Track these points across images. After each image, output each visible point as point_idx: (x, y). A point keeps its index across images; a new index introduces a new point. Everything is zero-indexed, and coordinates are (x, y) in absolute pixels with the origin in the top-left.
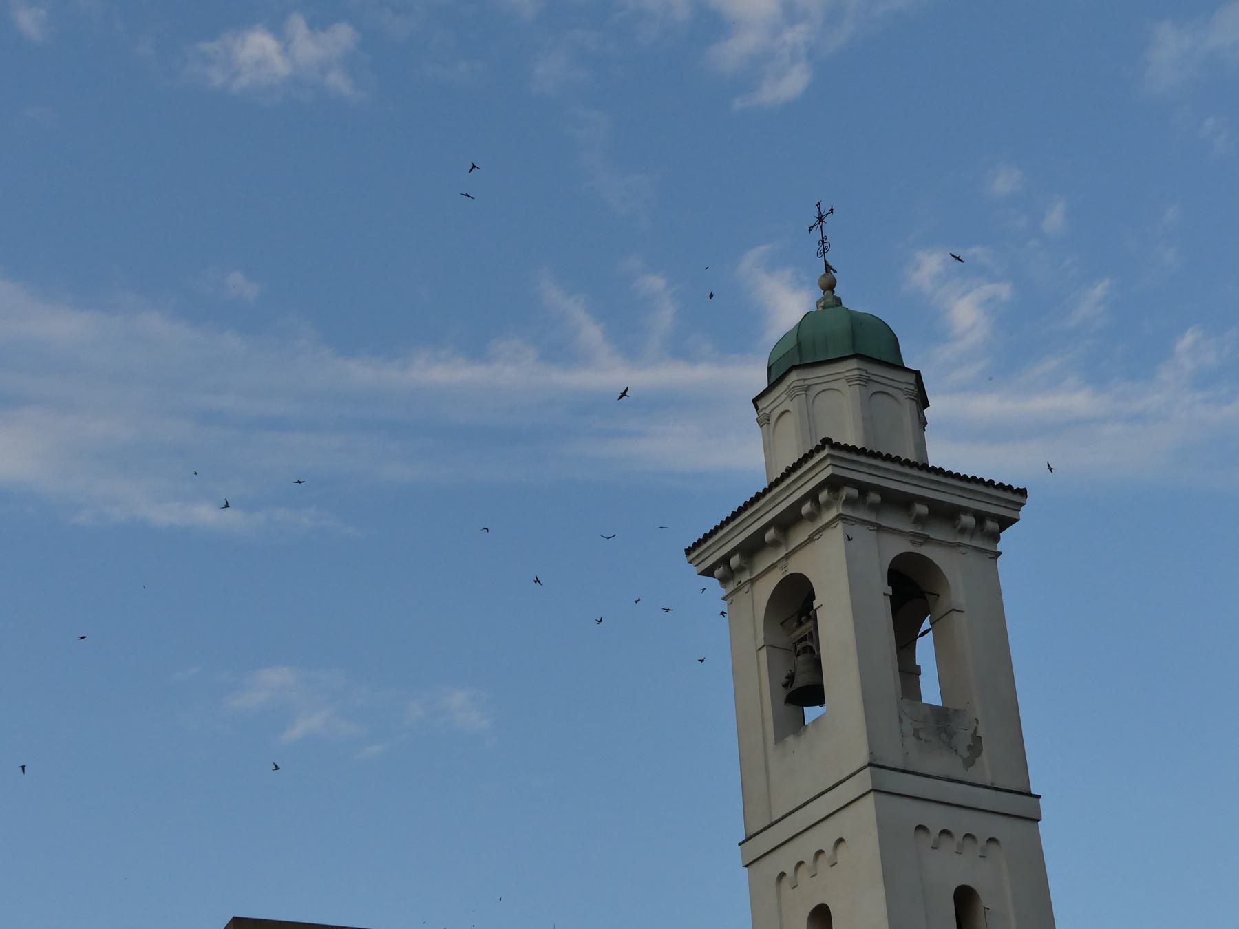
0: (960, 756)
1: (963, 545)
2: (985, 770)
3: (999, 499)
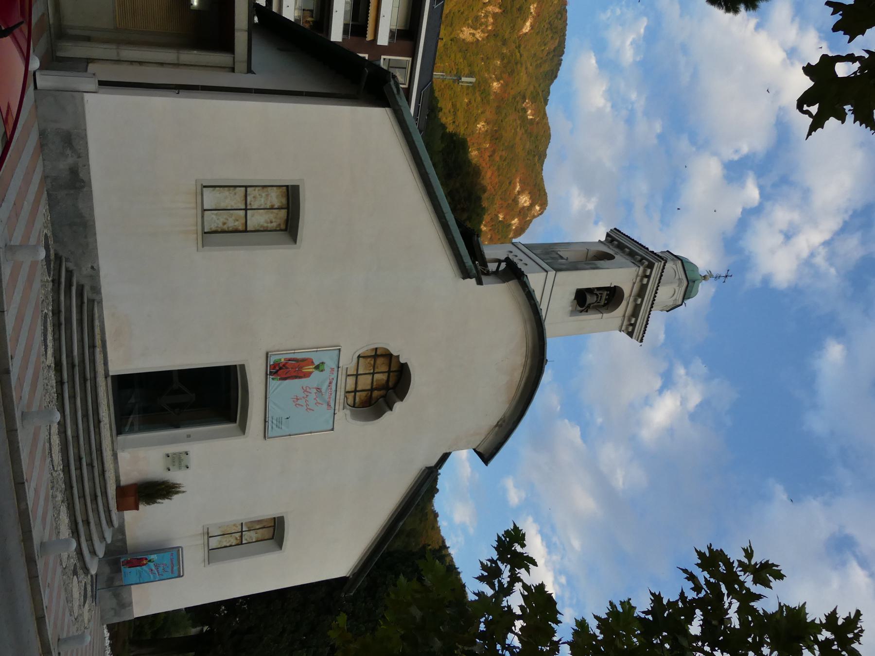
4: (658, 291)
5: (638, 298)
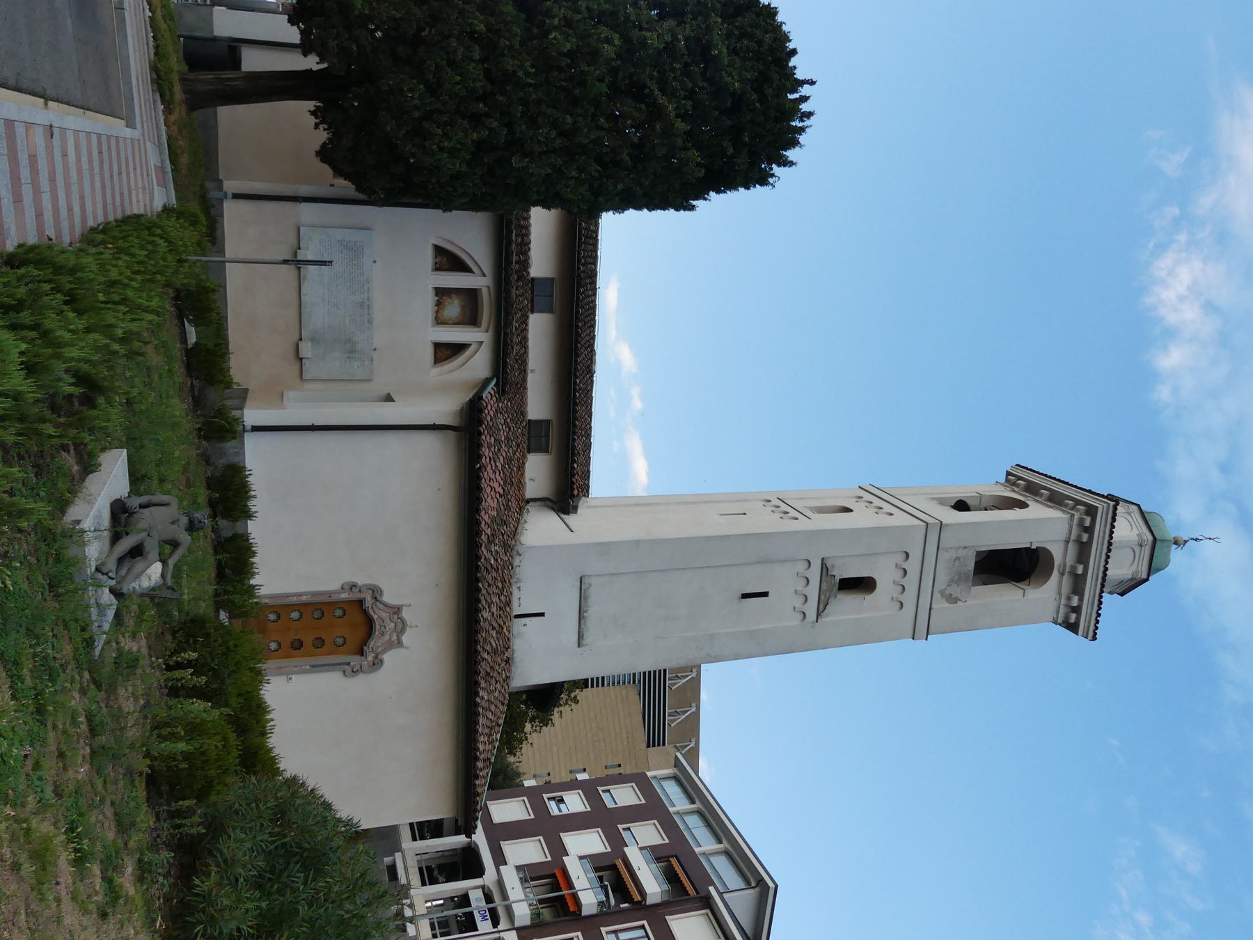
0: (946, 588)
1: (1060, 598)
2: (940, 605)
3: (1089, 627)
4: (1108, 560)
5: (1072, 596)
